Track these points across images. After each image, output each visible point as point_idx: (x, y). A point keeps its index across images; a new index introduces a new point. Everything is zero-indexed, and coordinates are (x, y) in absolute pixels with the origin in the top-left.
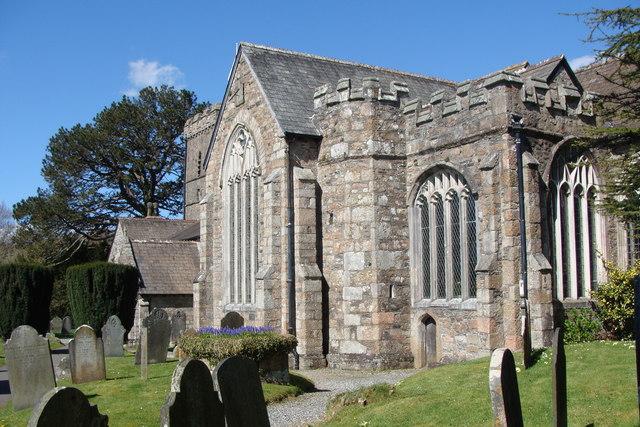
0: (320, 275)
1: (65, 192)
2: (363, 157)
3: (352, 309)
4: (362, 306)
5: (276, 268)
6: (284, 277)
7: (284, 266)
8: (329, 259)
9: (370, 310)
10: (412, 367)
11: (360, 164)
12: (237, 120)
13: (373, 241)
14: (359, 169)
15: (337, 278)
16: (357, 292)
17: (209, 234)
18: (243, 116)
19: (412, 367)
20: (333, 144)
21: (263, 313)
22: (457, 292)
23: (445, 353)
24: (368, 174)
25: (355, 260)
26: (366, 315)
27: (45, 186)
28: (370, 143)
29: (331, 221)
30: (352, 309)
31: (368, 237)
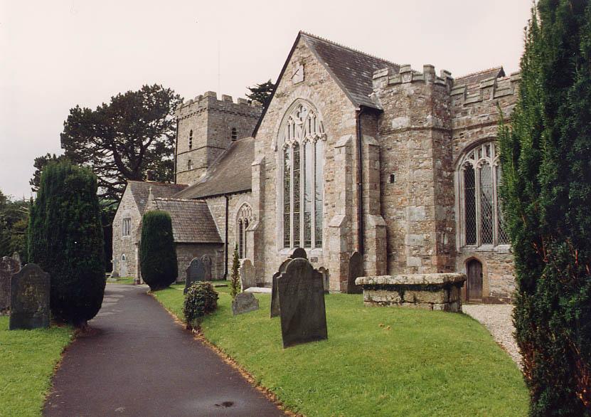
0: (385, 224)
1: (72, 157)
2: (424, 128)
3: (414, 252)
4: (423, 250)
5: (349, 218)
6: (355, 226)
7: (355, 217)
8: (392, 211)
9: (430, 254)
10: (289, 247)
11: (421, 134)
12: (295, 95)
13: (432, 197)
14: (420, 139)
15: (402, 226)
16: (420, 238)
17: (263, 189)
18: (302, 93)
19: (289, 247)
20: (394, 118)
21: (339, 255)
22: (487, 239)
23: (492, 289)
24: (427, 143)
25: (419, 212)
26: (427, 258)
27: (60, 152)
28: (429, 117)
29: (392, 181)
30: (414, 252)
31: (376, 188)
